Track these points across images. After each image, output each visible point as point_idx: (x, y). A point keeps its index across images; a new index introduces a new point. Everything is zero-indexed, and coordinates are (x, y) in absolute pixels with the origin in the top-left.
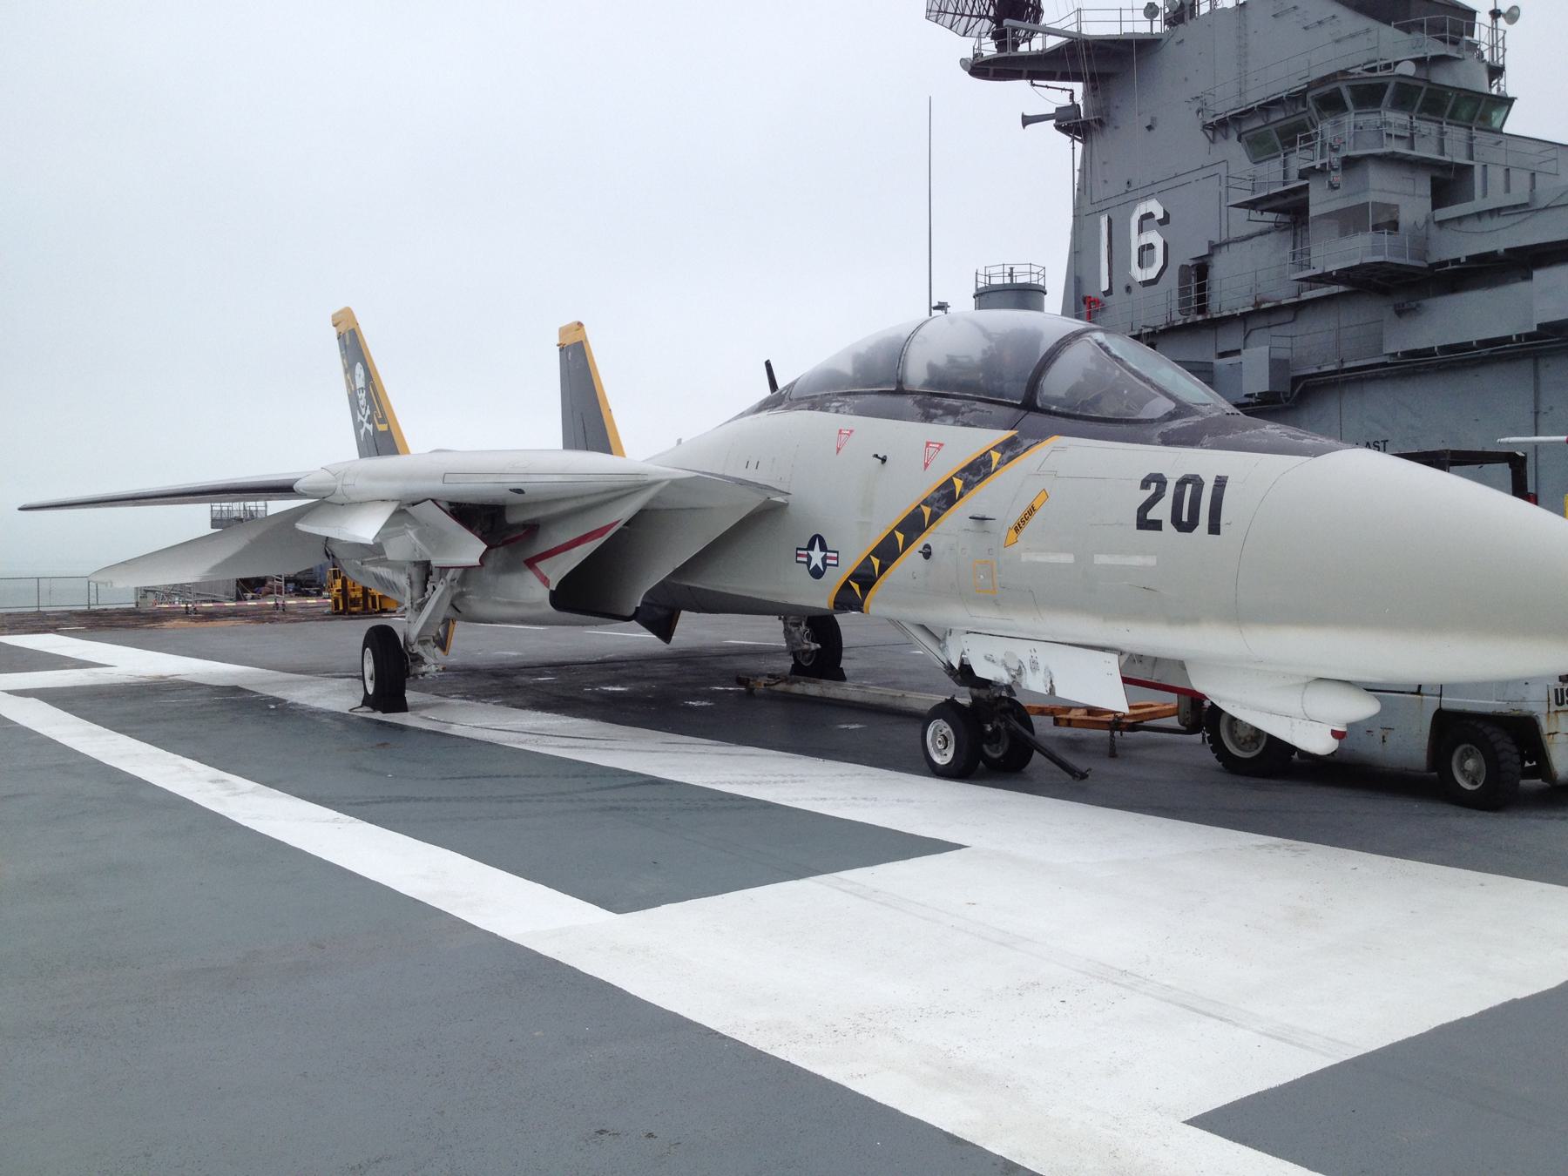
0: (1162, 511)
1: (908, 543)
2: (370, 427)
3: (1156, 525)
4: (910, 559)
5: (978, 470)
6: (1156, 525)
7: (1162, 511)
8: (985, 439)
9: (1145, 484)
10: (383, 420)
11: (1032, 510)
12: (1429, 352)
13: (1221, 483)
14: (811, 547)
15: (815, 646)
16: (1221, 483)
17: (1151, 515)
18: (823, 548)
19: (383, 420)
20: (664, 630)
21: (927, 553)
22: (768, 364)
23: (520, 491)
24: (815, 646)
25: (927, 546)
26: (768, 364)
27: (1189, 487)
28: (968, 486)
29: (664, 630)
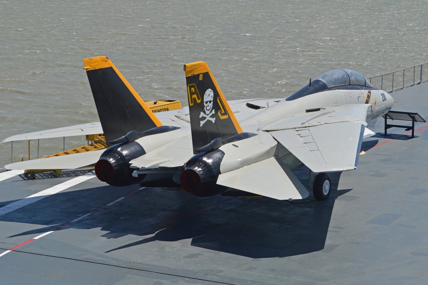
10: (226, 113)
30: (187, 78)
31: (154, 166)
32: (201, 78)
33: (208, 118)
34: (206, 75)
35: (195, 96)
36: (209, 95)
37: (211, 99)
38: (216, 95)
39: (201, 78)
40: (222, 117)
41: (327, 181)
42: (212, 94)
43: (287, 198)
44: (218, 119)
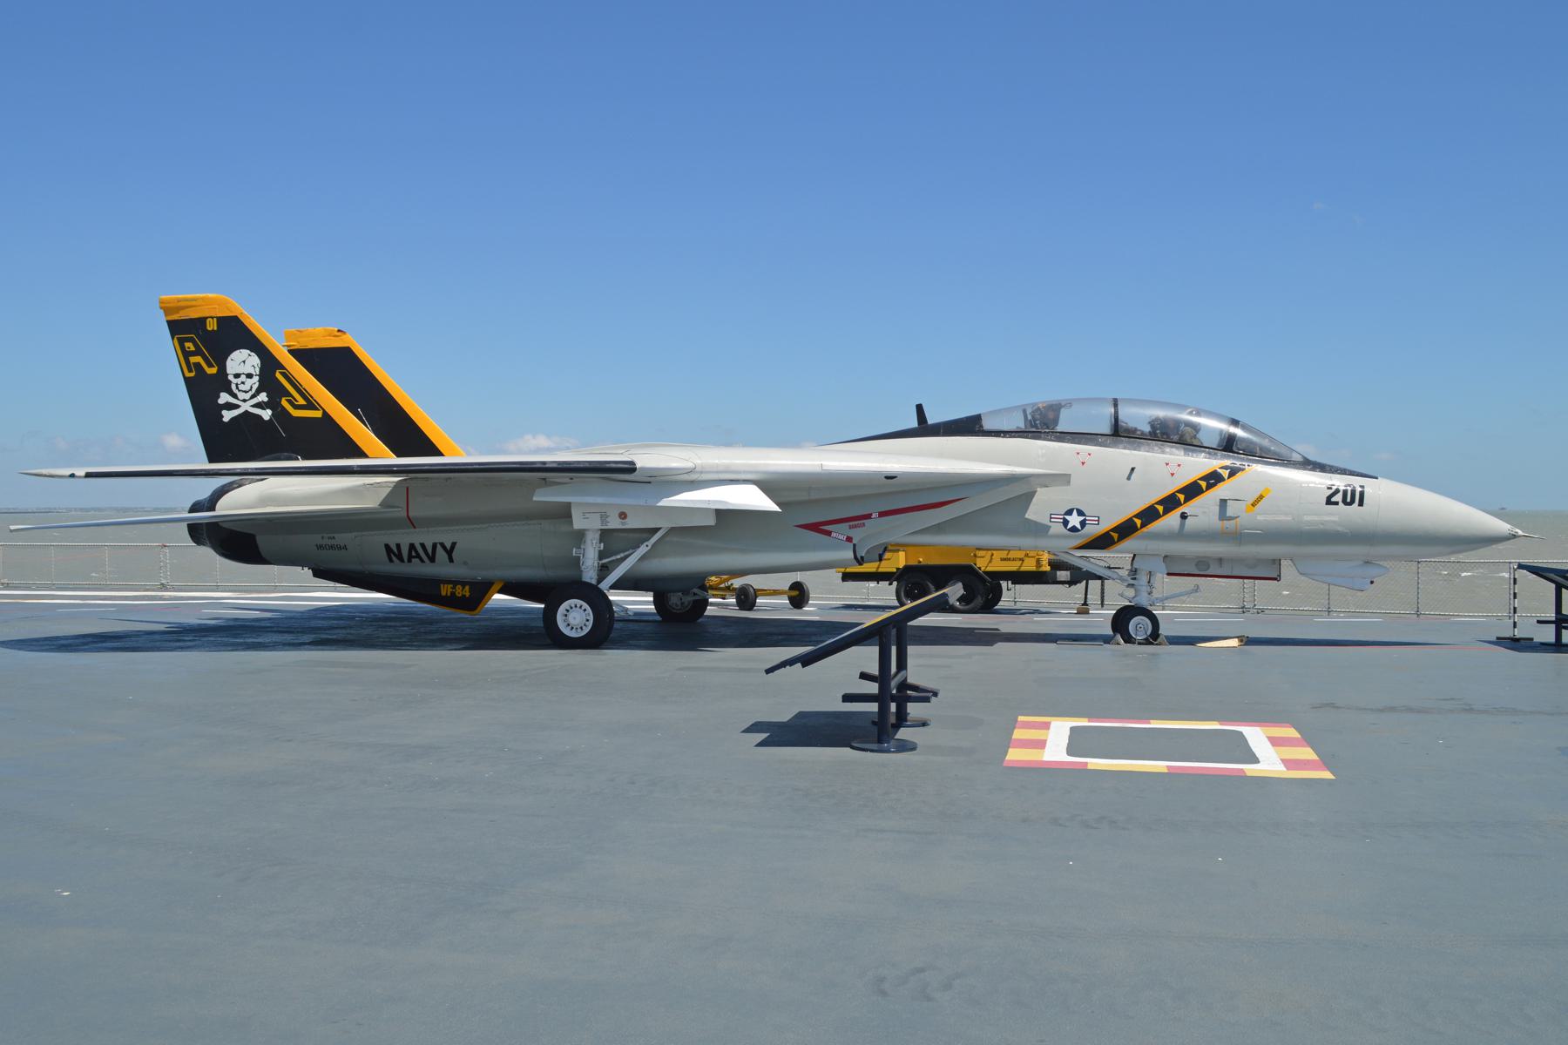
1: (1166, 511)
4: (1171, 520)
5: (1214, 479)
11: (1261, 497)
18: (1080, 513)
28: (1209, 487)
31: (692, 471)
44: (280, 413)
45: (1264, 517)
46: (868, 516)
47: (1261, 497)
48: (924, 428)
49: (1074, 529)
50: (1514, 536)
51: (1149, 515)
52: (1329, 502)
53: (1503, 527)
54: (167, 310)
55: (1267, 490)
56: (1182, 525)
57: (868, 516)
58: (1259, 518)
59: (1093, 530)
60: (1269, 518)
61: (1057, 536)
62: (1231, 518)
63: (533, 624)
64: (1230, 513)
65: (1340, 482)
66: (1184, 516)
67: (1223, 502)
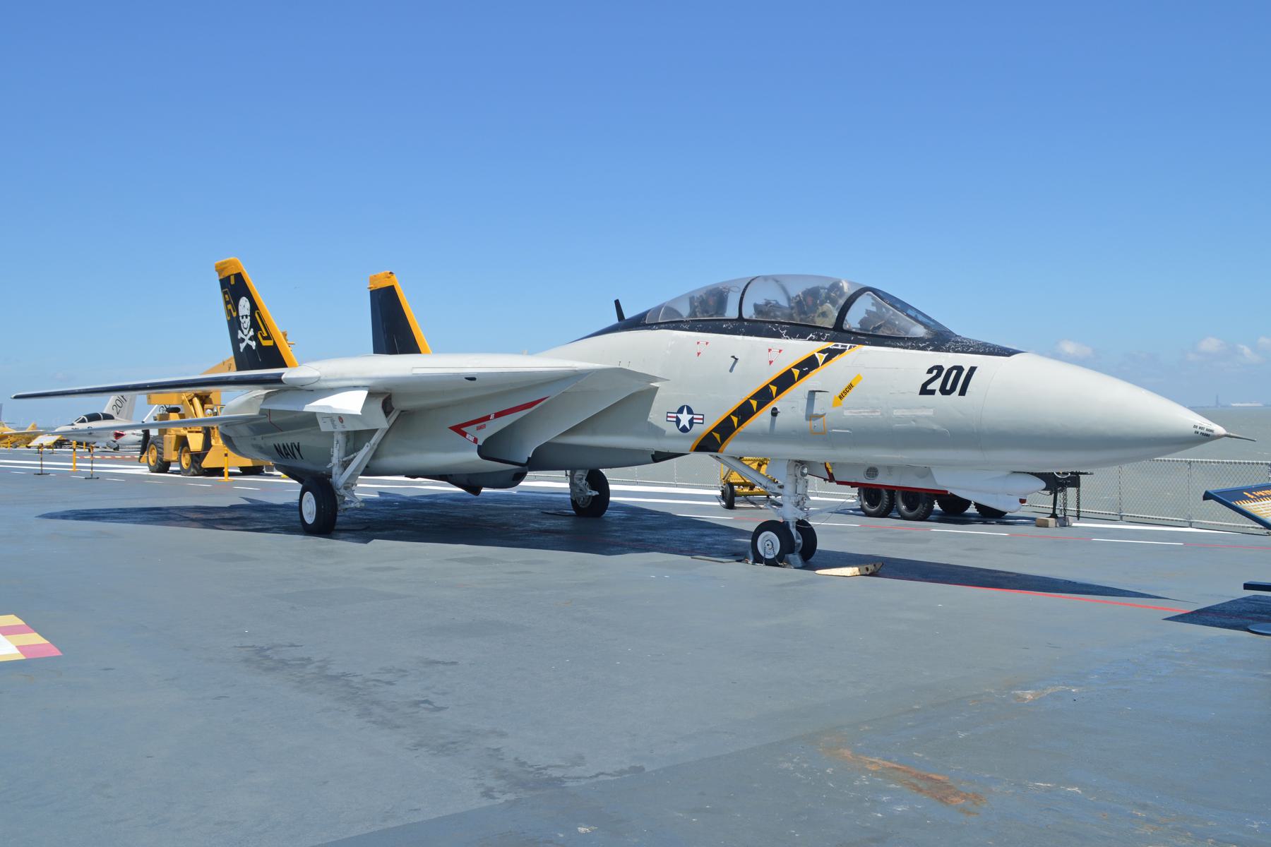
0: (936, 386)
1: (760, 407)
2: (253, 344)
3: (932, 392)
4: (762, 418)
5: (809, 364)
6: (932, 392)
7: (936, 386)
8: (796, 349)
9: (930, 371)
10: (268, 338)
11: (851, 386)
12: (792, 335)
13: (973, 369)
14: (681, 411)
15: (595, 493)
16: (973, 369)
17: (930, 387)
18: (690, 411)
19: (268, 338)
20: (474, 490)
21: (775, 413)
22: (617, 303)
23: (473, 379)
24: (595, 493)
25: (775, 409)
26: (617, 303)
27: (954, 372)
28: (802, 375)
29: (474, 490)
30: (221, 281)
31: (319, 379)
32: (233, 282)
33: (247, 341)
34: (239, 276)
35: (230, 307)
36: (244, 305)
37: (248, 313)
38: (254, 307)
39: (233, 282)
40: (265, 343)
41: (310, 519)
42: (248, 305)
43: (376, 543)
44: (259, 344)
45: (851, 412)
46: (487, 418)
47: (851, 386)
48: (626, 324)
49: (684, 430)
50: (1207, 437)
51: (745, 412)
52: (924, 391)
53: (1187, 419)
54: (220, 269)
55: (858, 378)
56: (773, 422)
57: (487, 418)
58: (847, 413)
59: (701, 430)
60: (907, 413)
61: (673, 437)
62: (818, 417)
63: (560, 501)
64: (817, 410)
65: (948, 360)
66: (775, 413)
67: (812, 393)
